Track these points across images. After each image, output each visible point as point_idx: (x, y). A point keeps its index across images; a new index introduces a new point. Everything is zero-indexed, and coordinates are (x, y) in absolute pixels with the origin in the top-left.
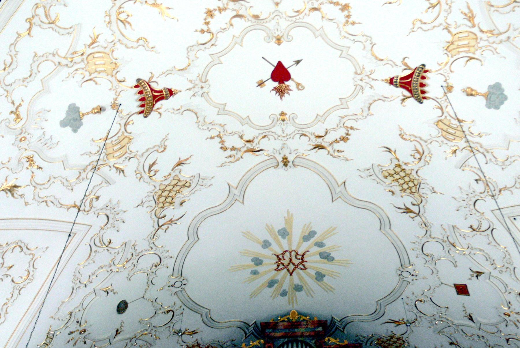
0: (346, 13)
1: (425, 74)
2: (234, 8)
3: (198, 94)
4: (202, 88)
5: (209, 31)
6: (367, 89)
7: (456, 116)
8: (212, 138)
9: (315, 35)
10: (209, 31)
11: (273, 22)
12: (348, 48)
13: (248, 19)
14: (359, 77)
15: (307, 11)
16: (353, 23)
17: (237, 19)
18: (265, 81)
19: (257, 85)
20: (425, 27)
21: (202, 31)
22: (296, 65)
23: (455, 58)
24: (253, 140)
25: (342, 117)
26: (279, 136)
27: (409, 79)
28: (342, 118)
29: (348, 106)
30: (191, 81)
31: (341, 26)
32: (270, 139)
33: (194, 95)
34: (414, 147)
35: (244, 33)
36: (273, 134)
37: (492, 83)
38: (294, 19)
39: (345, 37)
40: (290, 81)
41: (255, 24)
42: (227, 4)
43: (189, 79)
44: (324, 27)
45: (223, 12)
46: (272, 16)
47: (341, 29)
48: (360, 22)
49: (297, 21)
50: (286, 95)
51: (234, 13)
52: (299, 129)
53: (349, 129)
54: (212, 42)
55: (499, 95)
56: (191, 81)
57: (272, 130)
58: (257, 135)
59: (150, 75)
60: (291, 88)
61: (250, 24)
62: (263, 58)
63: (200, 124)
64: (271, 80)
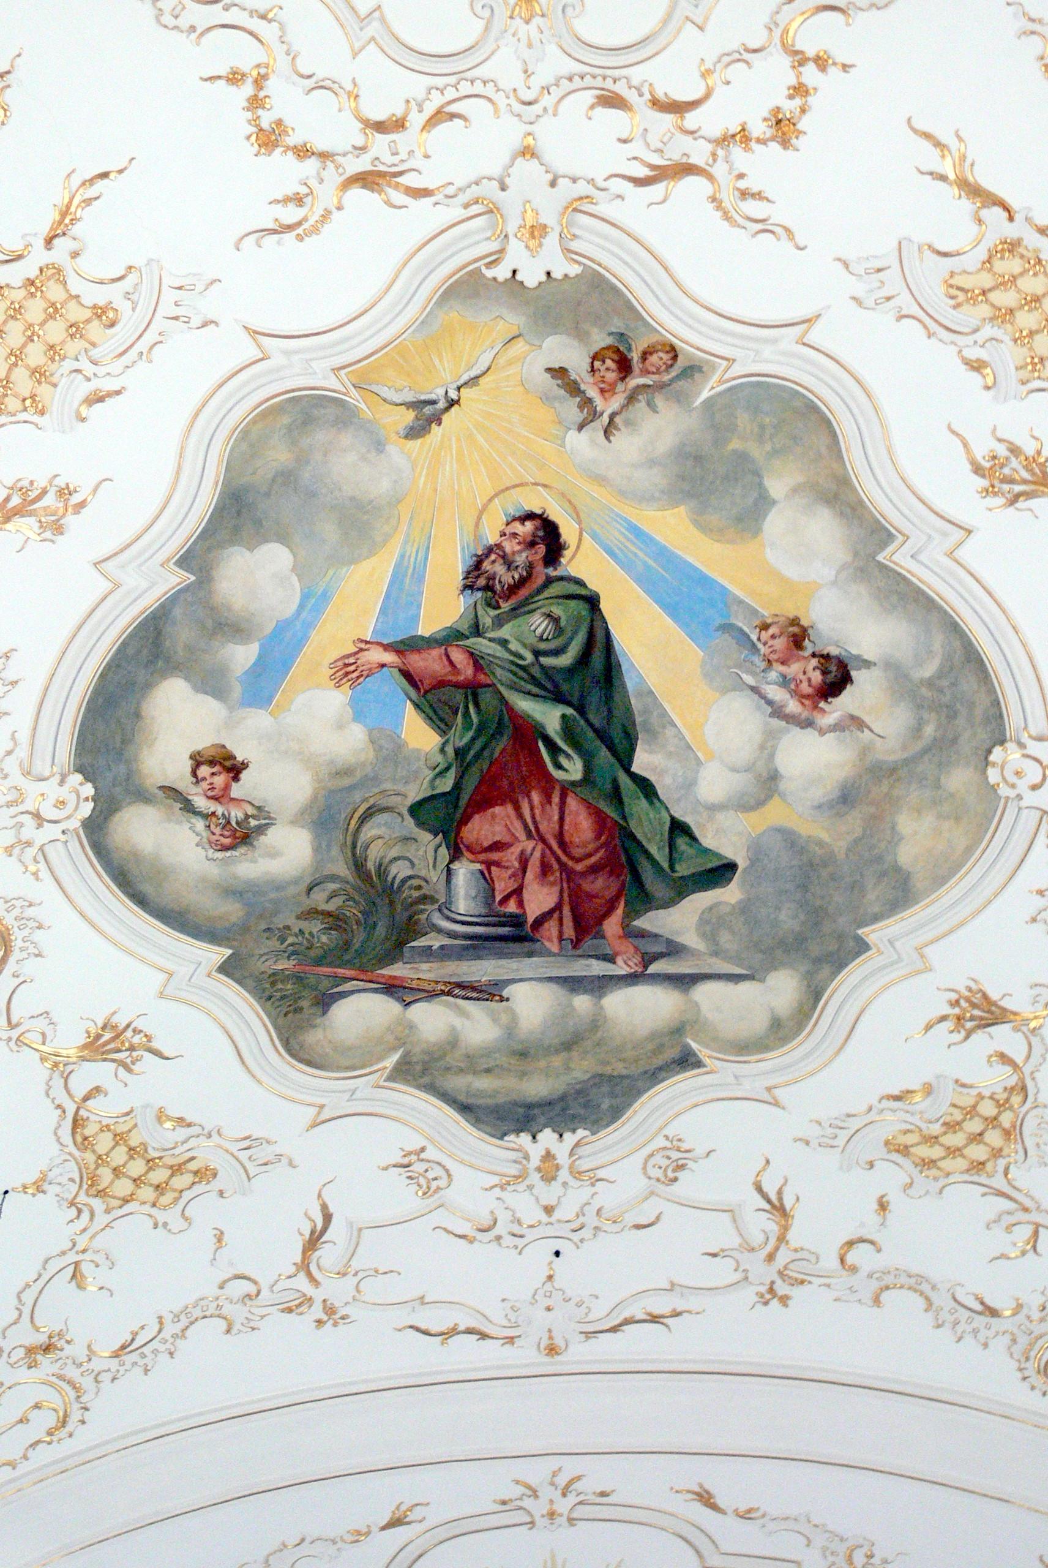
0: (266, 119)
2: (689, 139)
5: (800, 59)
7: (982, 1303)
9: (383, 20)
10: (800, 59)
11: (544, 75)
13: (641, 95)
15: (416, 120)
16: (235, 78)
21: (822, 62)
31: (282, 63)
35: (661, 41)
38: (465, 88)
39: (263, 17)
41: (617, 73)
42: (715, 160)
45: (734, 128)
46: (547, 101)
47: (279, 50)
49: (452, 80)
51: (692, 119)
61: (637, 74)
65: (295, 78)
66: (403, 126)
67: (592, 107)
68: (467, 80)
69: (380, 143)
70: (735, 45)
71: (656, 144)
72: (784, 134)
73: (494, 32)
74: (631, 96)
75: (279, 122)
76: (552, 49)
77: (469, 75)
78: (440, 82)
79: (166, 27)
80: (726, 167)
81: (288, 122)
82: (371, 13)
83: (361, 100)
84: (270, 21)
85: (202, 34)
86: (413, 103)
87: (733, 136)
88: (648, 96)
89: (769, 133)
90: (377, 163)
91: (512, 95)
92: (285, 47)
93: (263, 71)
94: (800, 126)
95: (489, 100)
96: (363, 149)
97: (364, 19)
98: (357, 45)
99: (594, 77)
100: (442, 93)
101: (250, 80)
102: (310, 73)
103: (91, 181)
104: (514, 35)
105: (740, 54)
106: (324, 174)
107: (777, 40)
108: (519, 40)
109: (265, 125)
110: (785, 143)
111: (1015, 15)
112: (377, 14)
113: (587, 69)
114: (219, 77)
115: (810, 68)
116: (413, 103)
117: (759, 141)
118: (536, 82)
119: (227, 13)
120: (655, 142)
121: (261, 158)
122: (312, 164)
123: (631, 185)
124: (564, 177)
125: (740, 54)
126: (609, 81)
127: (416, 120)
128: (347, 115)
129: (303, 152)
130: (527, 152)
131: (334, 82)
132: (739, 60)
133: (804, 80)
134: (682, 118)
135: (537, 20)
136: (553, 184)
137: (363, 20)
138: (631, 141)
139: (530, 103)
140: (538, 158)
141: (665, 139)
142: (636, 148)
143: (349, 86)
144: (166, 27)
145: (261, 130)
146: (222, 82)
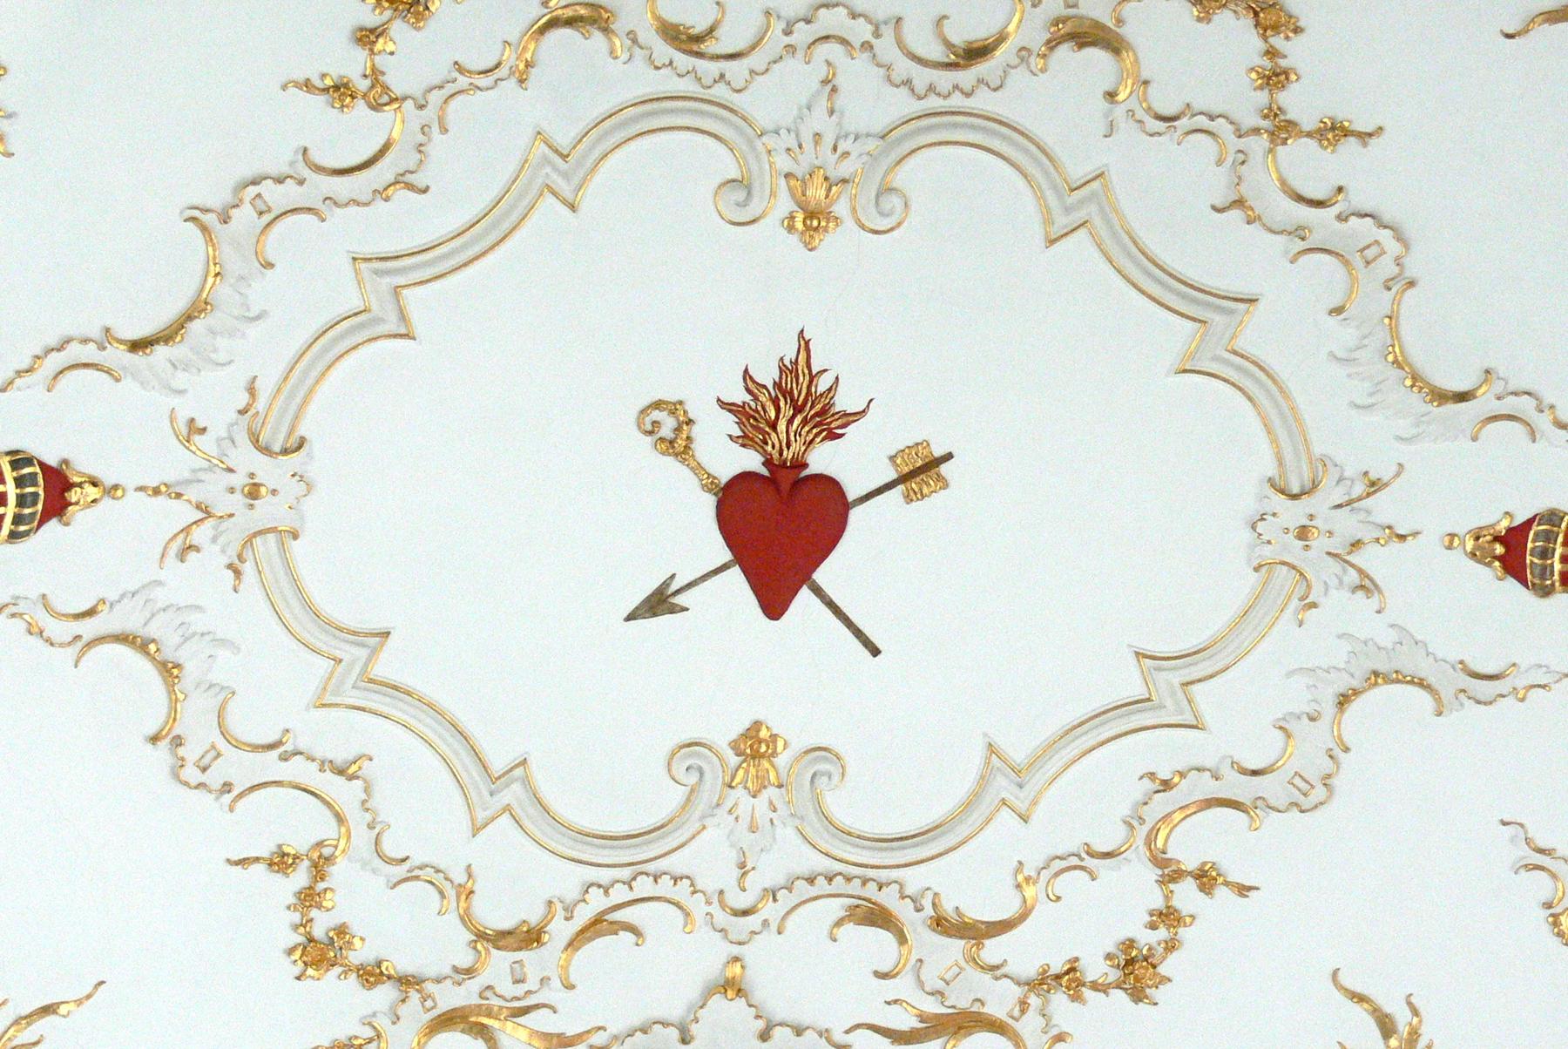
0: (321, 925)
2: (987, 977)
3: (1341, 489)
4: (1303, 533)
5: (1171, 874)
6: (219, 414)
8: (1333, 132)
9: (527, 782)
10: (1171, 874)
11: (768, 872)
14: (268, 511)
15: (560, 931)
16: (281, 862)
17: (981, 911)
18: (888, 486)
19: (944, 469)
21: (1206, 879)
22: (666, 584)
24: (1052, 44)
25: (410, 187)
26: (867, 46)
28: (402, 181)
29: (357, 272)
30: (1366, 586)
31: (362, 839)
32: (929, 27)
33: (1375, 486)
35: (963, 831)
36: (904, 67)
38: (644, 887)
39: (341, 772)
40: (725, 474)
41: (883, 875)
42: (1023, 1012)
43: (1374, 602)
44: (465, 826)
45: (1057, 967)
49: (626, 873)
50: (767, 375)
51: (993, 950)
52: (720, 92)
53: (364, 85)
54: (1162, 804)
56: (1366, 586)
57: (904, 104)
58: (1019, 77)
59: (1522, 871)
60: (730, 424)
61: (915, 879)
62: (875, 652)
63: (1386, 267)
64: (852, 492)
65: (377, 862)
66: (538, 940)
67: (839, 923)
68: (647, 874)
69: (499, 964)
70: (1074, 845)
71: (933, 983)
72: (1137, 979)
73: (700, 807)
74: (903, 911)
75: (341, 930)
76: (787, 833)
77: (651, 867)
78: (604, 876)
79: (186, 784)
80: (1041, 1022)
81: (356, 928)
82: (512, 769)
83: (475, 899)
84: (352, 778)
85: (241, 796)
86: (559, 906)
87: (1058, 977)
88: (929, 911)
89: (1114, 975)
90: (488, 994)
91: (715, 899)
92: (368, 817)
93: (326, 851)
94: (1163, 969)
95: (677, 905)
96: (469, 972)
97: (497, 779)
98: (481, 816)
99: (849, 879)
100: (606, 892)
101: (306, 863)
102: (401, 856)
103: (30, 1018)
104: (730, 812)
105: (1082, 859)
106: (403, 1010)
107: (1140, 842)
108: (737, 819)
109: (319, 932)
110: (1138, 995)
111: (1513, 840)
112: (519, 772)
113: (839, 867)
114: (257, 860)
115: (1187, 888)
116: (559, 906)
117: (1095, 986)
118: (756, 883)
119: (283, 764)
120: (932, 980)
121: (307, 983)
122: (385, 994)
123: (887, 1041)
124: (780, 1024)
125: (1082, 859)
126: (872, 886)
127: (560, 931)
128: (453, 918)
129: (371, 975)
130: (732, 987)
131: (438, 871)
132: (1075, 868)
133: (1176, 902)
134: (979, 946)
135: (771, 792)
136: (764, 1036)
137: (496, 780)
138: (894, 976)
139: (745, 913)
140: (746, 996)
141: (947, 977)
142: (902, 987)
143: (460, 878)
144: (186, 784)
145: (311, 940)
146: (260, 868)
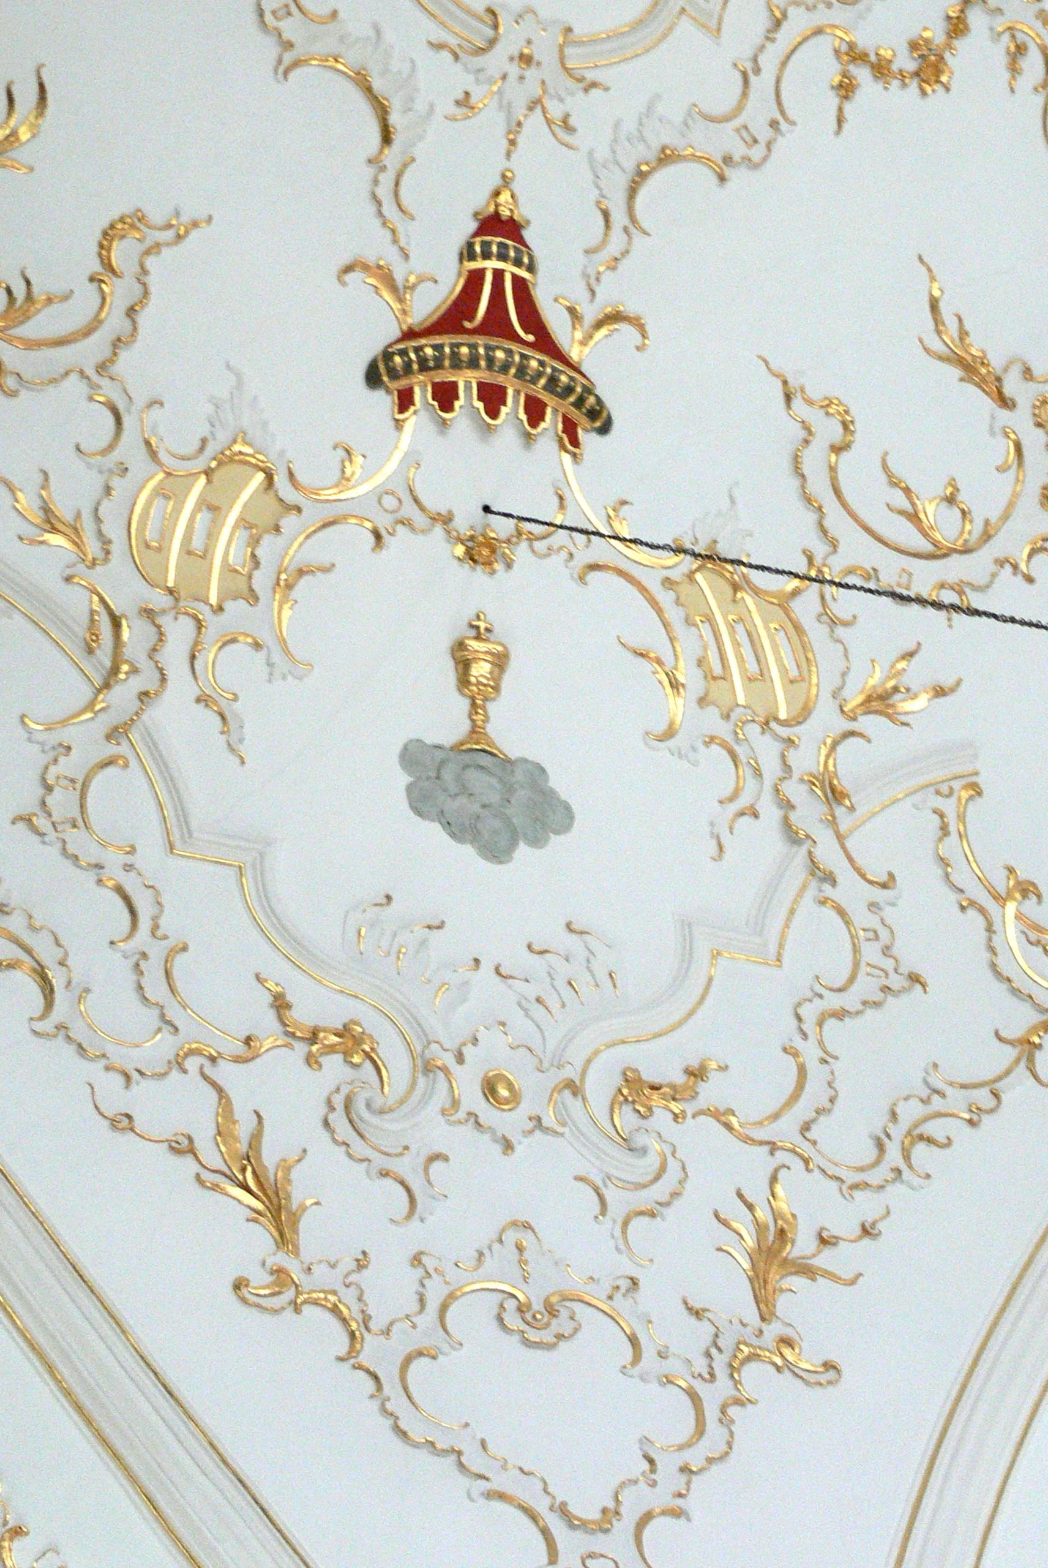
0: (906, 62)
1: (551, 422)
12: (713, 24)
14: (545, 50)
16: (846, 89)
20: (815, 460)
23: (665, 598)
27: (526, 332)
34: (57, 287)
37: (559, 782)
39: (778, 24)
48: (846, 127)
55: (507, 822)
